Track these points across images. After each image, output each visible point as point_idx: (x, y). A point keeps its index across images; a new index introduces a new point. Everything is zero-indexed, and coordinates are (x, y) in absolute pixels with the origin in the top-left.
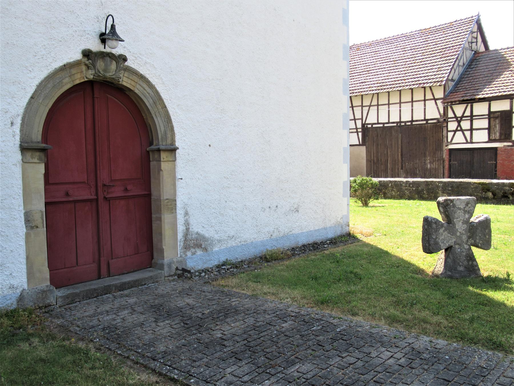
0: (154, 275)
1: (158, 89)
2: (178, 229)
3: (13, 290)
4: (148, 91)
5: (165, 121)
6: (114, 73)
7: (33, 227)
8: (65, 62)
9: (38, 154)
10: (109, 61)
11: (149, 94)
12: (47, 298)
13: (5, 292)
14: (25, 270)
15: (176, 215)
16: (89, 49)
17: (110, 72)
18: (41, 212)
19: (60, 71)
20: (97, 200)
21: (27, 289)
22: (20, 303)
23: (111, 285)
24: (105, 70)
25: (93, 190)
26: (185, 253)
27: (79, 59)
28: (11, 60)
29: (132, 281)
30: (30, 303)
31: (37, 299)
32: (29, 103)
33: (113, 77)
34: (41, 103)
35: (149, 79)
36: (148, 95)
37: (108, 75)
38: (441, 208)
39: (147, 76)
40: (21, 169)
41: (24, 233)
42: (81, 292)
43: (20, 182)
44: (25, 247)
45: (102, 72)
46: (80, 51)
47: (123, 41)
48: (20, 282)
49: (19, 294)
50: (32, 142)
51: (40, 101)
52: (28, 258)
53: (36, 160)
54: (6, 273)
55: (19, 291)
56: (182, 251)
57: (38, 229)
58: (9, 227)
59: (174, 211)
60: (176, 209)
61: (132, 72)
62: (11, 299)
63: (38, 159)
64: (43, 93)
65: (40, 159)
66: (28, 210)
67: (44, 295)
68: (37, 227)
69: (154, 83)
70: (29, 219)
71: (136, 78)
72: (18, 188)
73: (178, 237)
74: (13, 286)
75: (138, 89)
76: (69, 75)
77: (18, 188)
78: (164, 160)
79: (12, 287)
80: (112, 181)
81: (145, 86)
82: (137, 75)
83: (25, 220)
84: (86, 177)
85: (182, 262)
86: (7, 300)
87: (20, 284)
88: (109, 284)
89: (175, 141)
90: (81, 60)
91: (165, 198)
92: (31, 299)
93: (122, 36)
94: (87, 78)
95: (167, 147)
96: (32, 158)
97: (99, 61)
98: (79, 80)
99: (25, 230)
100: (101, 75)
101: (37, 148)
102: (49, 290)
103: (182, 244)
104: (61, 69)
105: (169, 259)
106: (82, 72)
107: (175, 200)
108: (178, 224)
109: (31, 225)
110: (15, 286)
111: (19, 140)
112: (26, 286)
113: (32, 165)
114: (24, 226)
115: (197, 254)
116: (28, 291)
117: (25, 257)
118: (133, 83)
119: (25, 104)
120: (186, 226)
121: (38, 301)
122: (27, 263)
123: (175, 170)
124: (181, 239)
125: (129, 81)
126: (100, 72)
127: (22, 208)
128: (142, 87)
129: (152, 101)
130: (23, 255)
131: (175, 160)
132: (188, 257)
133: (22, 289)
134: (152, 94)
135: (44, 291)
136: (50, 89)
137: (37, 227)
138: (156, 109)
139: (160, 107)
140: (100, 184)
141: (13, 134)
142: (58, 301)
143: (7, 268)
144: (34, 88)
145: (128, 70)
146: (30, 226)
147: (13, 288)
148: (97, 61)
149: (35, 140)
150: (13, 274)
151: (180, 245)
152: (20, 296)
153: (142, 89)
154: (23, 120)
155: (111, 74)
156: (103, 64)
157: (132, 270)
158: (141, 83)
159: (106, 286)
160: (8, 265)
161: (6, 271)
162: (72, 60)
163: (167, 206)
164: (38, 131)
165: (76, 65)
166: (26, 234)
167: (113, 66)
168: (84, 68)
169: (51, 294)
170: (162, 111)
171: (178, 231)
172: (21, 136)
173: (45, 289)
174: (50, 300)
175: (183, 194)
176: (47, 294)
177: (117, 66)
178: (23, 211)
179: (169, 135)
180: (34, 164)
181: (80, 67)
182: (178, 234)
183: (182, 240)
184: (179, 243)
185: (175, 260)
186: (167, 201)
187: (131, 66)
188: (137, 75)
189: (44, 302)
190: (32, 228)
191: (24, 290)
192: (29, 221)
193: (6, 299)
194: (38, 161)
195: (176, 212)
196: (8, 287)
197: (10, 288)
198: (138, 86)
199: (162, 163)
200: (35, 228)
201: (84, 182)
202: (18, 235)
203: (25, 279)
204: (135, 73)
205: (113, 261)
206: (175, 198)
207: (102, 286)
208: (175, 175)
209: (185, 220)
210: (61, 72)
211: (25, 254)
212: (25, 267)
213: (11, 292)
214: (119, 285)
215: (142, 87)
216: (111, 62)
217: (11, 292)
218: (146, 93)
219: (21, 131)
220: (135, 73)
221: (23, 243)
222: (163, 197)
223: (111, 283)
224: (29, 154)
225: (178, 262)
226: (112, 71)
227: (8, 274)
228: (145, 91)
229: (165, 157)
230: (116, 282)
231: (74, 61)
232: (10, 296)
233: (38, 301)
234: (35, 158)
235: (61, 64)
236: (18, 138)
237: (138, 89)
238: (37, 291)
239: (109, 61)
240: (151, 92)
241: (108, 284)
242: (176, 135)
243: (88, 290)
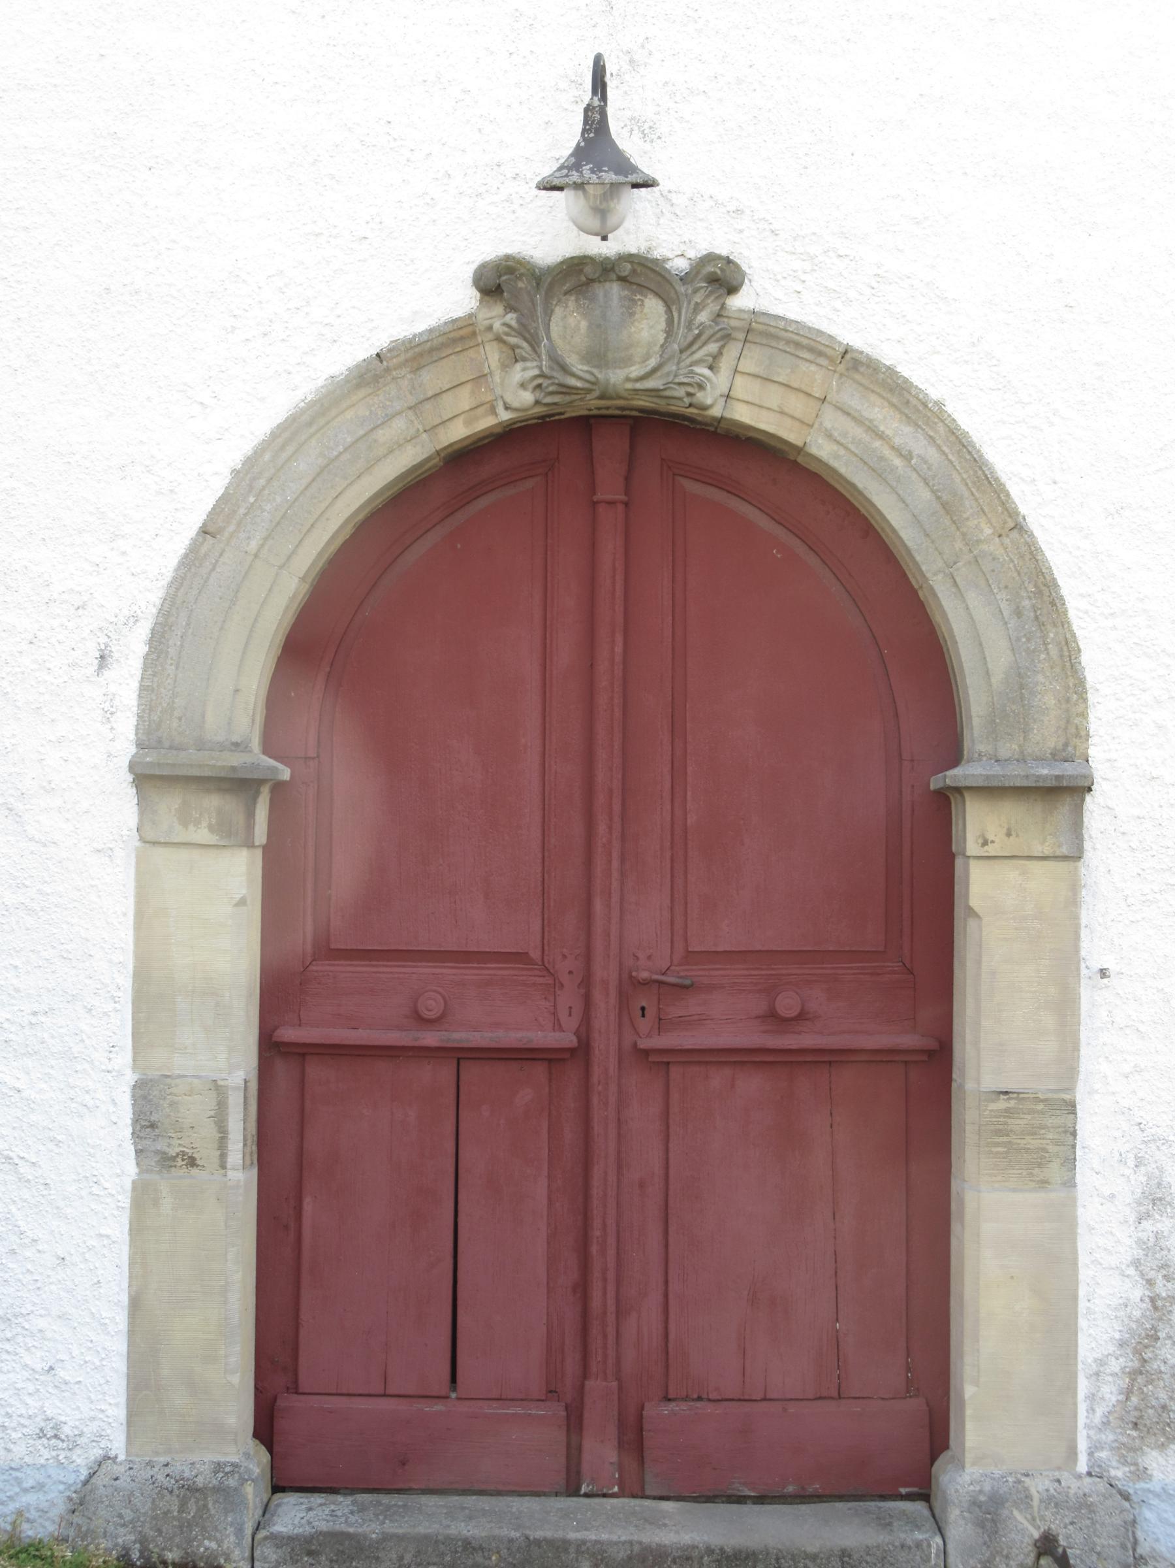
0: (868, 1550)
1: (965, 422)
2: (1082, 1292)
3: (55, 1448)
4: (897, 441)
5: (1018, 613)
6: (653, 362)
7: (174, 1158)
8: (381, 340)
9: (213, 802)
10: (615, 302)
11: (907, 457)
12: (204, 1529)
13: (20, 1450)
14: (121, 1365)
15: (1073, 1201)
16: (508, 257)
17: (627, 361)
18: (219, 1090)
19: (358, 386)
20: (582, 1052)
21: (122, 1457)
22: (76, 1519)
23: (566, 1543)
24: (598, 356)
25: (568, 998)
26: (1127, 1452)
27: (459, 312)
28: (117, 366)
29: (710, 1551)
30: (122, 1530)
31: (155, 1518)
32: (192, 560)
33: (650, 384)
34: (256, 556)
35: (904, 370)
36: (898, 462)
37: (616, 377)
38: (716, 1501)
39: (888, 354)
40: (132, 871)
41: (128, 1186)
42: (386, 1538)
43: (125, 936)
44: (125, 1250)
45: (579, 367)
46: (468, 273)
47: (647, 184)
48: (93, 1419)
49: (84, 1473)
50: (201, 745)
51: (253, 545)
52: (136, 1305)
53: (202, 834)
54: (28, 1359)
55: (82, 1461)
56: (1109, 1437)
57: (194, 1171)
58: (58, 1143)
59: (1054, 1171)
60: (1070, 1162)
61: (789, 342)
62: (40, 1487)
63: (211, 828)
64: (268, 507)
65: (223, 828)
66: (153, 1074)
67: (192, 1507)
68: (192, 1162)
69: (934, 394)
70: (154, 1117)
71: (819, 375)
72: (110, 961)
73: (1083, 1341)
74: (56, 1427)
75: (829, 436)
76: (412, 401)
77: (110, 961)
78: (991, 850)
79: (51, 1433)
80: (690, 957)
81: (878, 412)
82: (821, 354)
83: (135, 1121)
84: (536, 926)
85: (1090, 1508)
86: (26, 1491)
87: (94, 1427)
88: (560, 1534)
89: (1083, 735)
90: (471, 316)
91: (989, 1082)
92: (128, 1515)
93: (646, 166)
94: (507, 408)
95: (997, 770)
96: (185, 820)
97: (558, 312)
98: (468, 423)
99: (131, 1168)
100: (579, 384)
101: (196, 772)
102: (217, 1490)
103: (1110, 1393)
104: (361, 376)
105: (997, 1473)
106: (481, 378)
107: (1071, 1108)
108: (1083, 1259)
109: (161, 1145)
110: (66, 1430)
111: (132, 736)
112: (118, 1445)
113: (184, 854)
114: (130, 1150)
115: (1014, 1479)
116: (119, 1470)
117: (125, 1298)
118: (797, 405)
119: (172, 562)
120: (1150, 1283)
121: (159, 1531)
122: (131, 1333)
123: (1076, 918)
124: (1101, 1362)
125: (774, 397)
126: (565, 369)
127: (124, 1059)
128: (858, 421)
129: (926, 494)
130: (117, 1290)
131: (1076, 856)
132: (1155, 1485)
133: (96, 1453)
134: (932, 454)
135: (190, 1490)
136: (305, 482)
137: (192, 1162)
138: (959, 545)
139: (988, 531)
140: (605, 972)
141: (107, 706)
142: (257, 1553)
143: (32, 1335)
144: (218, 486)
145: (761, 333)
146: (157, 1152)
147: (56, 1436)
148: (549, 313)
149: (220, 738)
150: (62, 1373)
151: (1092, 1398)
152: (86, 1483)
153: (858, 432)
154: (158, 639)
155: (635, 371)
156: (584, 324)
157: (790, 1489)
158: (850, 396)
159: (538, 1543)
160: (42, 1323)
161: (28, 1349)
162: (421, 326)
163: (998, 1133)
164: (237, 691)
165: (443, 346)
166: (134, 1189)
167: (644, 325)
168: (493, 355)
169: (226, 1512)
170: (1000, 552)
171: (1082, 1305)
172: (140, 717)
173: (200, 1482)
174: (220, 1543)
175: (1138, 1070)
176: (205, 1506)
177: (670, 322)
178: (130, 1077)
179: (1048, 700)
180: (196, 854)
181: (471, 353)
182: (1082, 1323)
183: (1115, 1366)
184: (1083, 1386)
185: (1038, 1486)
186: (1002, 1104)
187: (778, 310)
188: (821, 354)
189: (190, 1541)
190: (166, 1161)
191: (107, 1458)
192: (153, 1126)
193: (19, 1481)
194: (213, 839)
195: (1070, 1184)
196: (32, 1429)
197: (42, 1434)
198: (830, 419)
199: (973, 864)
200: (180, 1163)
201: (520, 957)
202: (95, 1189)
203: (117, 1411)
204: (811, 350)
205: (666, 1409)
206: (1071, 1089)
207: (514, 1534)
208: (1076, 949)
209: (1140, 1242)
210: (361, 393)
211: (125, 1285)
212: (120, 1346)
213: (46, 1454)
214: (622, 1555)
215: (858, 421)
216: (630, 309)
217: (46, 1454)
218: (887, 452)
219: (144, 689)
220: (811, 350)
221: (118, 1228)
222: (978, 1081)
223: (572, 1535)
224: (169, 803)
225: (1054, 1502)
226: (638, 353)
227: (38, 1367)
228: (877, 444)
229: (994, 831)
230: (604, 1536)
231: (431, 331)
232: (40, 1477)
233: (159, 1531)
234: (197, 823)
235: (363, 351)
236: (126, 728)
237: (829, 436)
238: (160, 1477)
239: (615, 302)
240: (918, 445)
241: (549, 1534)
242: (1092, 697)
243: (426, 1537)
